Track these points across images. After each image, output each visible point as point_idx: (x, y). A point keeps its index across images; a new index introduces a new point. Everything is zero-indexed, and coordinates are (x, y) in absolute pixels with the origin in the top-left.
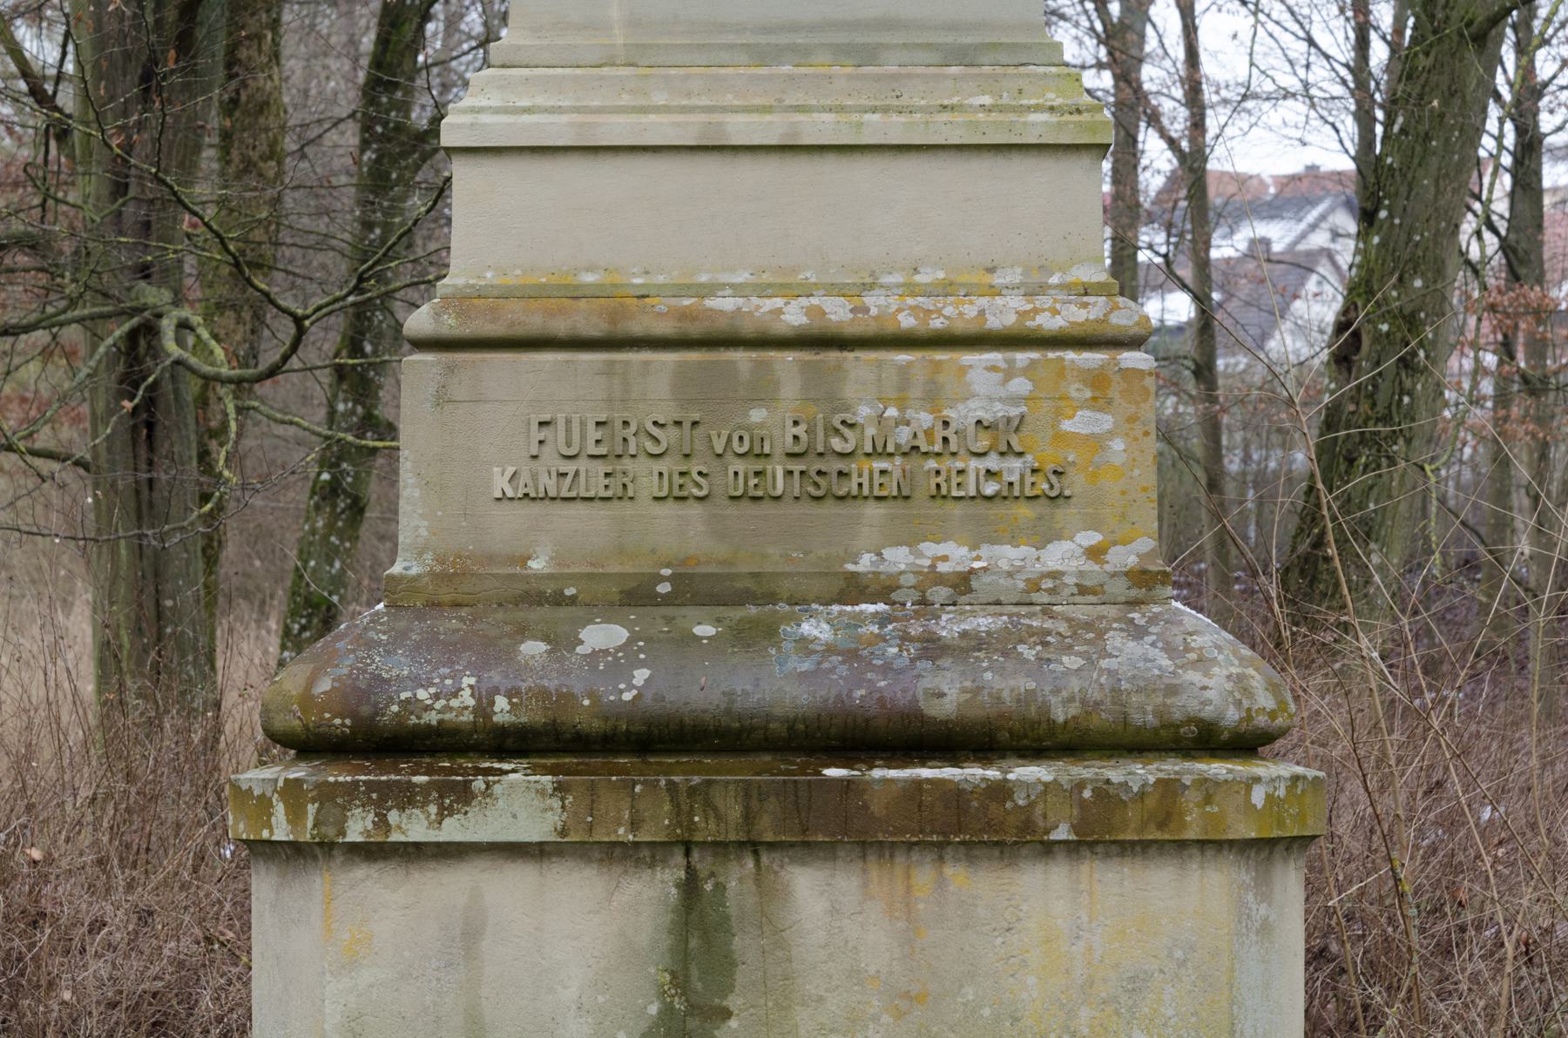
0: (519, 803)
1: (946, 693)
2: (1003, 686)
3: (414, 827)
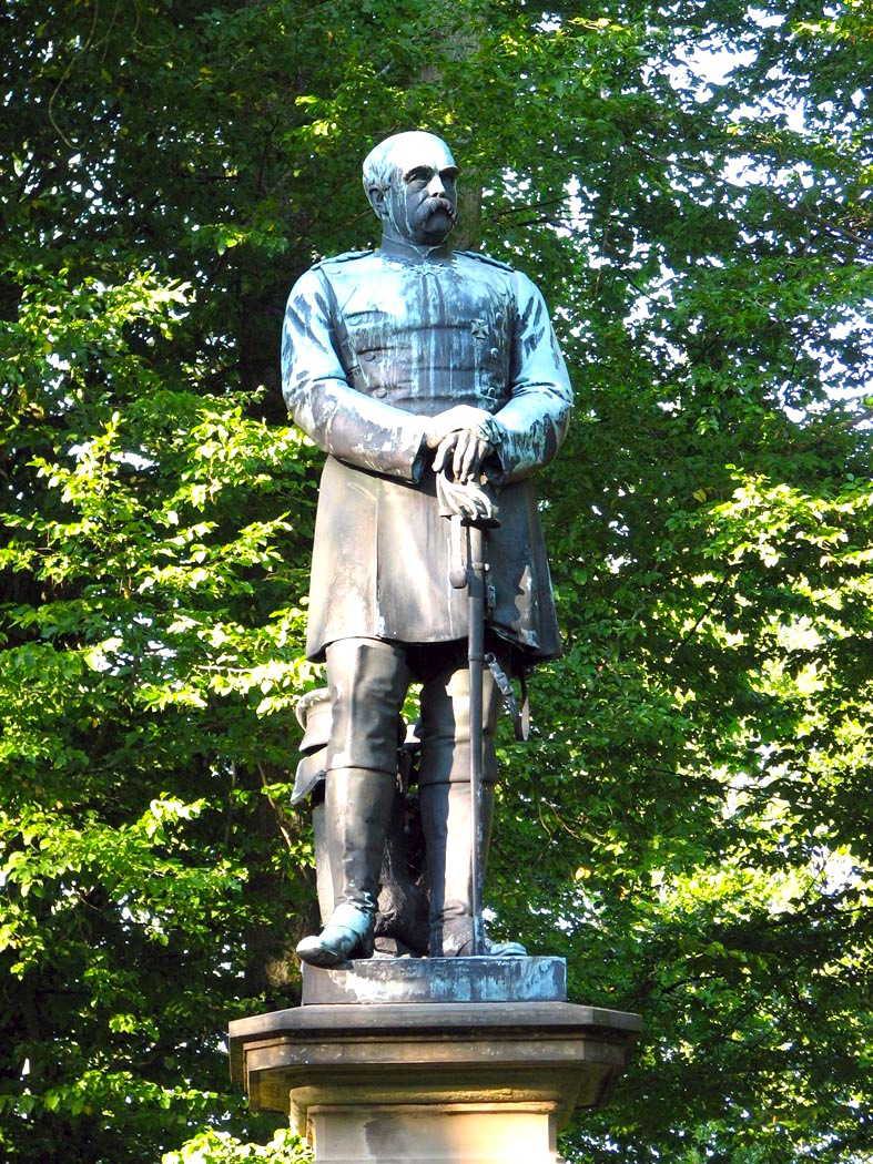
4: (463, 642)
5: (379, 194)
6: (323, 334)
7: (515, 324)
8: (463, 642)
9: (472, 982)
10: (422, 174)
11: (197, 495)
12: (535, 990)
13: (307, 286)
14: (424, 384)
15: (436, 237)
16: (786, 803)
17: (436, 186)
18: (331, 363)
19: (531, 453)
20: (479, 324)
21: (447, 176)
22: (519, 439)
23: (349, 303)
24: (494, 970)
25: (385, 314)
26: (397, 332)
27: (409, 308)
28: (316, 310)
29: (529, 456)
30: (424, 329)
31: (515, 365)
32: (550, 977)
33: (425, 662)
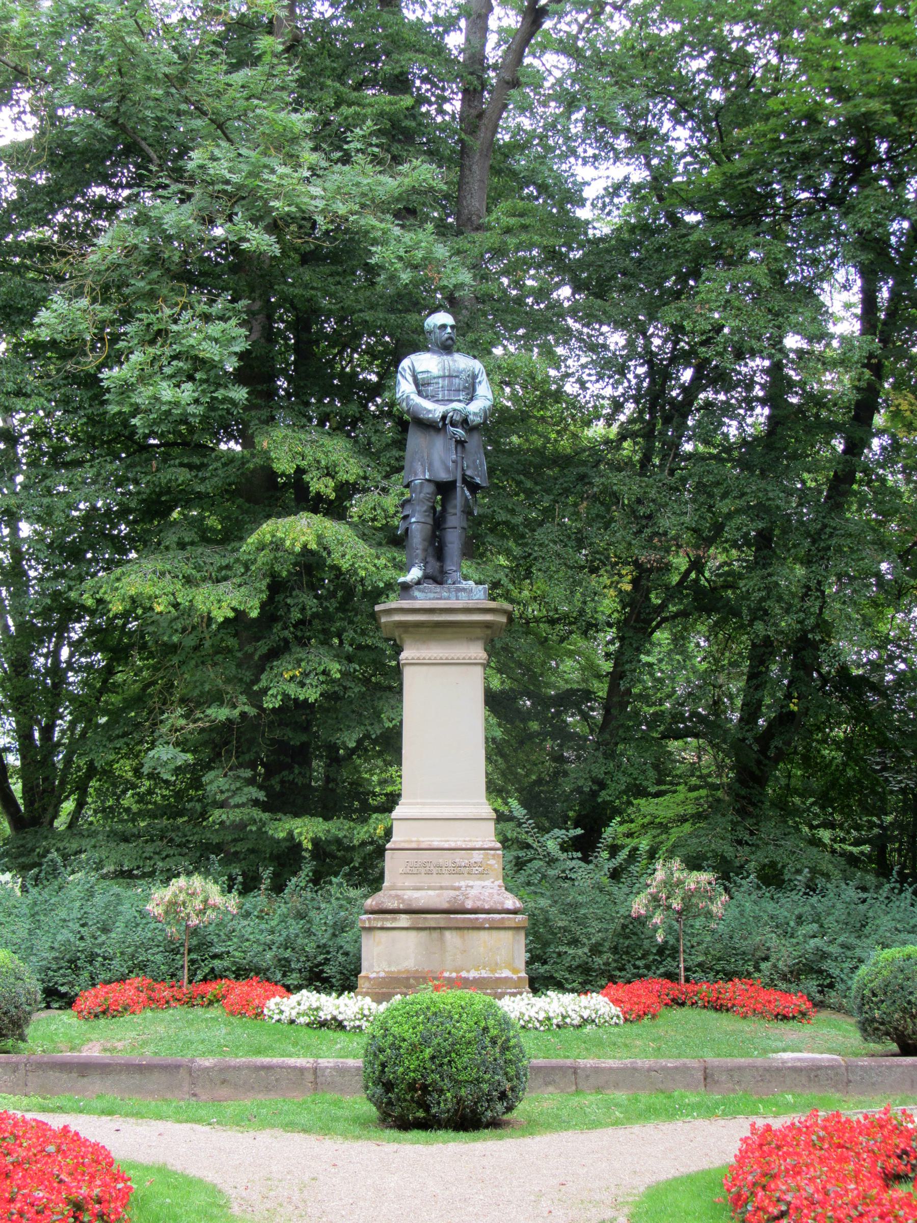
0: (404, 920)
1: (469, 905)
2: (479, 904)
3: (388, 925)
4: (454, 482)
5: (430, 332)
6: (410, 379)
7: (474, 377)
8: (454, 482)
10: (444, 327)
11: (175, 216)
13: (405, 363)
15: (446, 348)
16: (485, 655)
17: (449, 330)
18: (413, 388)
20: (463, 376)
21: (452, 327)
22: (475, 414)
23: (419, 369)
24: (464, 590)
29: (478, 420)
30: (444, 377)
31: (474, 390)
33: (444, 489)
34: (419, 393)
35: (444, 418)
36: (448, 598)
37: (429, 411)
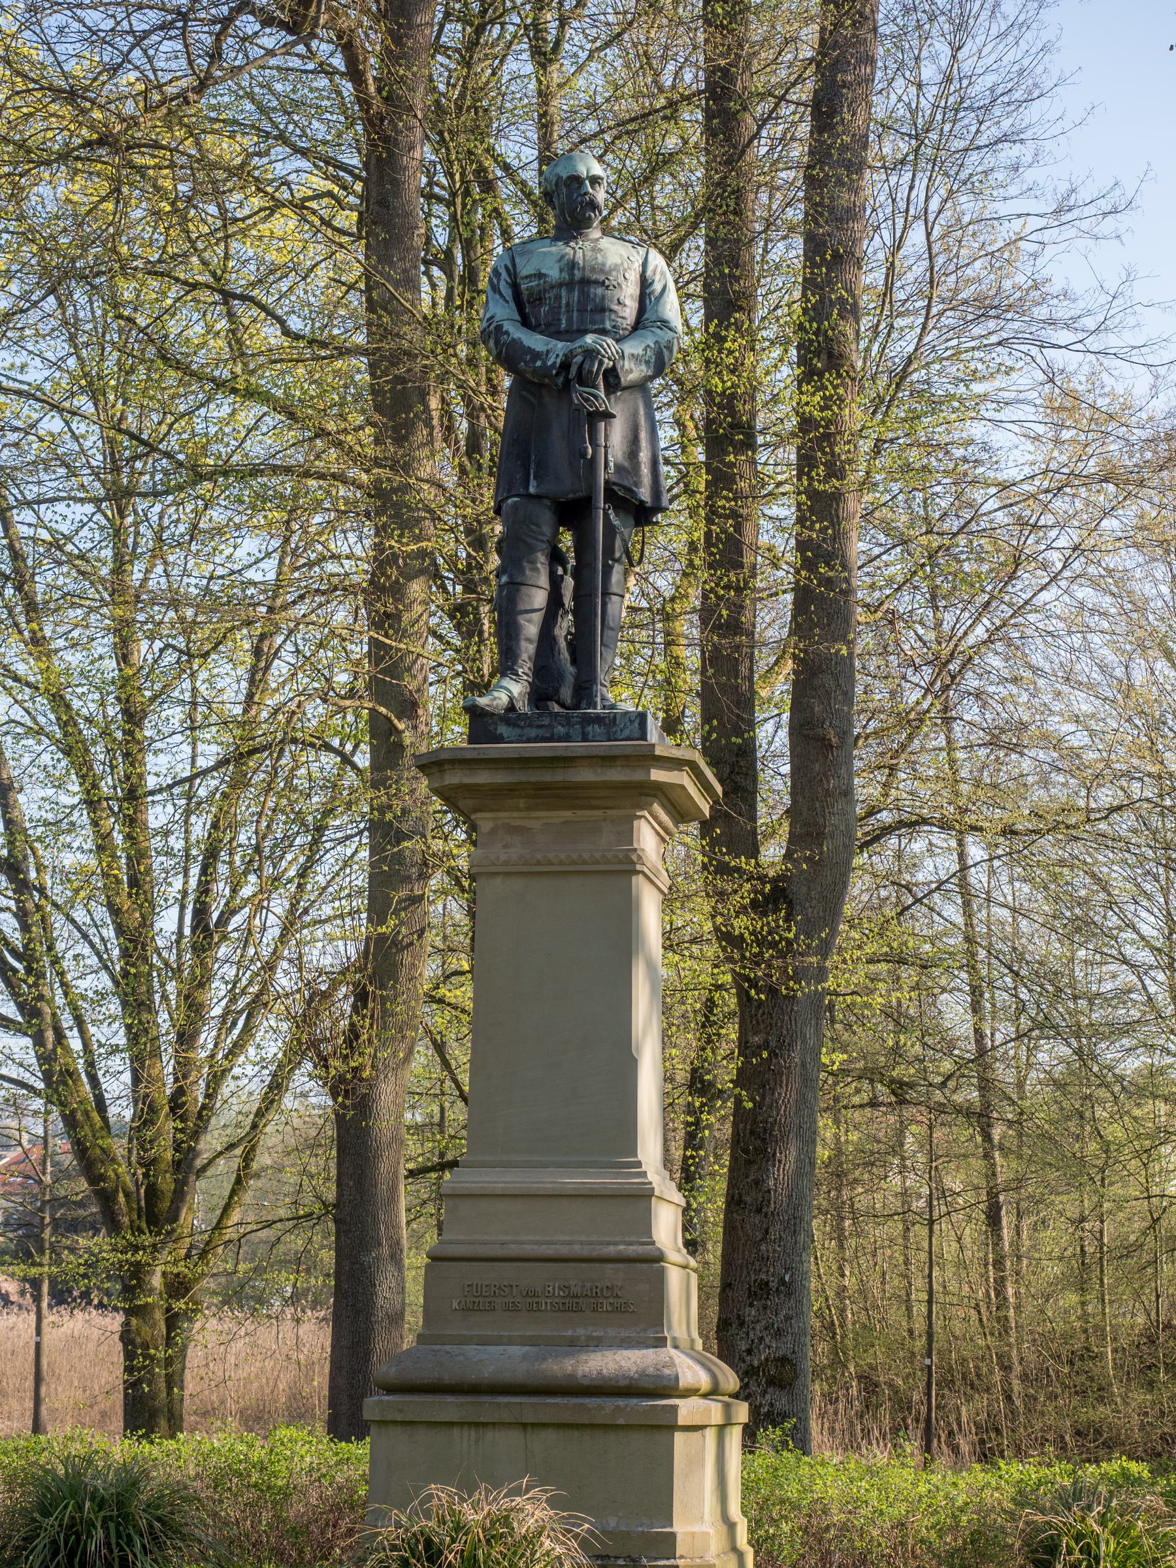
6: (507, 292)
9: (583, 728)
12: (626, 733)
14: (570, 320)
19: (644, 367)
25: (545, 275)
26: (552, 287)
27: (561, 270)
28: (504, 275)
32: (636, 724)
34: (525, 322)
35: (565, 366)
36: (567, 738)
37: (536, 355)
